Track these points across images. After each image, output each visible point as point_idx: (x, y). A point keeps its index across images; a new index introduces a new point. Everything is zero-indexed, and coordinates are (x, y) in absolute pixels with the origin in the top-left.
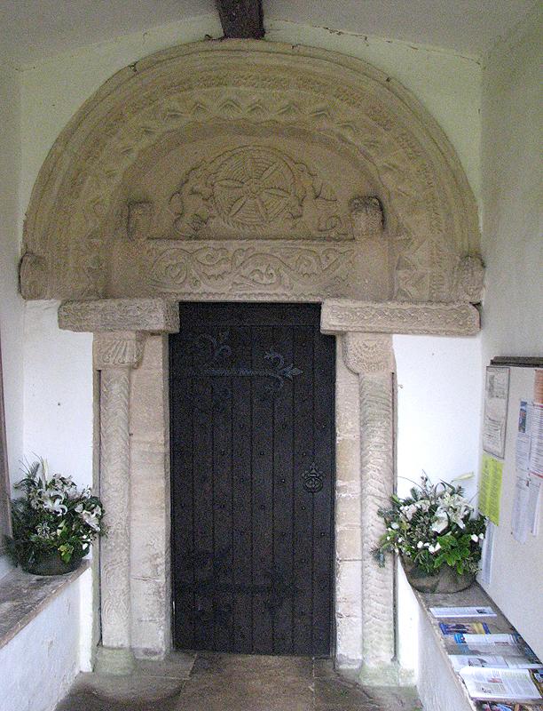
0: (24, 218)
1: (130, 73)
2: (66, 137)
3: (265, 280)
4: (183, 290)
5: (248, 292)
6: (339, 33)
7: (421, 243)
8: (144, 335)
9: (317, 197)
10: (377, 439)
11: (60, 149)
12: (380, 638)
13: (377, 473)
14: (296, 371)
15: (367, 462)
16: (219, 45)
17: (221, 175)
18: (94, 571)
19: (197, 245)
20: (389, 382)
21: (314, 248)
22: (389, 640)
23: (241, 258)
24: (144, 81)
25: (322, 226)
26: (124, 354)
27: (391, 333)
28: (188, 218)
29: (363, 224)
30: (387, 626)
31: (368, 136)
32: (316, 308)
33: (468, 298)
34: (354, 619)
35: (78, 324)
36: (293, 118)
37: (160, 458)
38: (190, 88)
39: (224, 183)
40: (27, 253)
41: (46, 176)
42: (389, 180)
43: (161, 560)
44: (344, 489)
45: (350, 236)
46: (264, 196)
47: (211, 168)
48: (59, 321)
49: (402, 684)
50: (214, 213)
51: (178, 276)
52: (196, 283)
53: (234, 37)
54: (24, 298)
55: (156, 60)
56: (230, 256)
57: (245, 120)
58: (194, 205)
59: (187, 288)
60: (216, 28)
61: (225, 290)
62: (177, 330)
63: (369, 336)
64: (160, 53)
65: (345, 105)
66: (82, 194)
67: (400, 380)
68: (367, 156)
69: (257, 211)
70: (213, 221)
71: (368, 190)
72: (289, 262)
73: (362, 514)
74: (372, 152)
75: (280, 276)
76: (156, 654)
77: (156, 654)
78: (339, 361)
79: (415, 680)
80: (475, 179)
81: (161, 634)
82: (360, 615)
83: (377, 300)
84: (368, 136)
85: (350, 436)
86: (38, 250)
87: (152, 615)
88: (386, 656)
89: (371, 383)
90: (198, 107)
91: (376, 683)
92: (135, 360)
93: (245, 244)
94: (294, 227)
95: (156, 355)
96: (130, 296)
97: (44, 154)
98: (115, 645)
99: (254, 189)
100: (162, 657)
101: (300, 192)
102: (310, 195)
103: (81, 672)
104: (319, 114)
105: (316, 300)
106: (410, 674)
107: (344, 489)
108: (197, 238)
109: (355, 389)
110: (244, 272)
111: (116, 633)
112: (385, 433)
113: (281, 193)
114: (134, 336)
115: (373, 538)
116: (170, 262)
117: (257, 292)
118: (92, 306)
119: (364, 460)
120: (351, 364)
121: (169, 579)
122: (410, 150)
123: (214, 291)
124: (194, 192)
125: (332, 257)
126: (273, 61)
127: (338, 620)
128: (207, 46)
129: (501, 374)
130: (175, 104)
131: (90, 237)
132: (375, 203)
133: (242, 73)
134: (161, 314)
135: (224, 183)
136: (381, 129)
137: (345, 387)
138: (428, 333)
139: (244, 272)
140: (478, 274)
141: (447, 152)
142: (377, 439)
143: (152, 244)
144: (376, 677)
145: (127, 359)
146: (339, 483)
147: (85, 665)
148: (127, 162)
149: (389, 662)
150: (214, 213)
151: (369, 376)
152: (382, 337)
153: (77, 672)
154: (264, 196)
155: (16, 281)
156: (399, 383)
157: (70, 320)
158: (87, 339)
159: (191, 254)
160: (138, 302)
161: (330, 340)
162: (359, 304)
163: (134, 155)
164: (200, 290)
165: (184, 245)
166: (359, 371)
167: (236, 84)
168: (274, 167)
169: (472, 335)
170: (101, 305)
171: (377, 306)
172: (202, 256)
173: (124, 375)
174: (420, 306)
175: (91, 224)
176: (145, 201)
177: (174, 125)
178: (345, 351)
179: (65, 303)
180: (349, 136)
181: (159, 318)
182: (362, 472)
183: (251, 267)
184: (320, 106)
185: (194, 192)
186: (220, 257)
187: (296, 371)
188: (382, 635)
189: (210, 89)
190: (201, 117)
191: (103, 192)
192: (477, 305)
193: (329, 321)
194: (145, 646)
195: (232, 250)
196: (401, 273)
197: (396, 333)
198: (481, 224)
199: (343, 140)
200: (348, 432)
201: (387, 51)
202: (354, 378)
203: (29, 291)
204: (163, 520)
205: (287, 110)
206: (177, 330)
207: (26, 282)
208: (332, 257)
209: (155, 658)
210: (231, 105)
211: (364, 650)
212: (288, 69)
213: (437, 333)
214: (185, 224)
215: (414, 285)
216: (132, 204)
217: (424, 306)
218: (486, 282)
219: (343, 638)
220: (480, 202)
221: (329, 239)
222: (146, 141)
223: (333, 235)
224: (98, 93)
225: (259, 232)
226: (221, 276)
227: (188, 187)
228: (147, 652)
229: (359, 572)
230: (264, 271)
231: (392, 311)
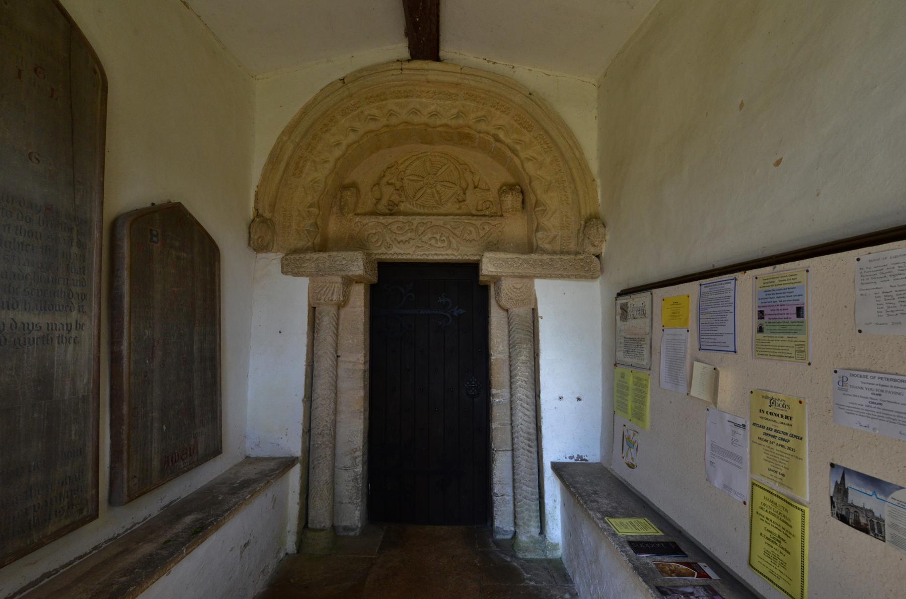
0: (256, 189)
1: (340, 84)
2: (290, 130)
3: (439, 244)
4: (380, 251)
5: (427, 253)
6: (494, 63)
7: (554, 213)
8: (349, 282)
9: (475, 187)
10: (523, 358)
11: (285, 138)
12: (530, 516)
13: (524, 383)
14: (462, 311)
15: (516, 375)
16: (406, 65)
17: (408, 172)
18: (302, 465)
19: (390, 219)
20: (531, 314)
21: (474, 222)
22: (536, 517)
23: (422, 229)
24: (352, 90)
25: (480, 208)
26: (333, 294)
27: (532, 277)
28: (384, 202)
29: (509, 203)
30: (535, 506)
31: (515, 136)
32: (475, 267)
33: (593, 250)
34: (507, 498)
35: (296, 270)
36: (461, 121)
37: (360, 374)
38: (386, 99)
39: (410, 177)
40: (258, 215)
41: (274, 159)
42: (530, 167)
43: (359, 453)
44: (497, 395)
45: (499, 214)
46: (439, 187)
47: (402, 167)
48: (282, 267)
49: (550, 556)
50: (404, 199)
51: (377, 241)
52: (389, 247)
53: (419, 59)
54: (255, 250)
55: (361, 74)
56: (414, 227)
57: (427, 125)
58: (388, 193)
59: (383, 250)
60: (405, 53)
61: (410, 251)
62: (375, 280)
63: (518, 280)
64: (361, 71)
65: (498, 113)
66: (304, 175)
67: (541, 312)
68: (514, 151)
69: (433, 196)
70: (402, 204)
71: (512, 180)
72: (456, 231)
73: (512, 415)
74: (518, 147)
75: (450, 242)
76: (353, 530)
77: (353, 530)
78: (493, 302)
79: (560, 553)
80: (594, 166)
81: (357, 513)
82: (512, 494)
83: (523, 253)
84: (515, 136)
85: (500, 356)
86: (267, 215)
87: (351, 498)
88: (535, 531)
89: (518, 316)
90: (391, 114)
91: (529, 556)
92: (342, 299)
93: (426, 219)
94: (460, 208)
95: (359, 298)
96: (339, 250)
97: (273, 142)
98: (318, 527)
99: (432, 182)
100: (358, 532)
101: (464, 185)
102: (471, 186)
103: (287, 554)
104: (479, 120)
105: (476, 258)
106: (555, 546)
107: (497, 395)
108: (391, 215)
109: (504, 321)
110: (424, 239)
111: (320, 515)
112: (529, 353)
113: (449, 184)
114: (340, 280)
115: (523, 434)
116: (371, 231)
117: (433, 252)
118: (308, 256)
119: (513, 373)
120: (503, 302)
121: (366, 467)
122: (545, 146)
123: (402, 252)
124: (388, 184)
125: (487, 228)
126: (448, 79)
127: (495, 498)
128: (395, 66)
129: (623, 300)
130: (375, 112)
131: (309, 207)
132: (518, 188)
133: (423, 89)
134: (361, 263)
135: (410, 177)
136: (525, 131)
137: (496, 317)
138: (561, 277)
139: (424, 239)
140: (601, 230)
141: (575, 145)
142: (523, 358)
143: (357, 219)
144: (527, 550)
145: (335, 298)
146: (494, 391)
147: (290, 545)
148: (338, 153)
149: (537, 536)
150: (404, 199)
151: (515, 311)
152: (526, 280)
153: (282, 555)
154: (439, 187)
155: (246, 235)
156: (540, 314)
157: (290, 268)
158: (303, 283)
159: (385, 226)
160: (344, 254)
161: (485, 288)
162: (509, 256)
163: (343, 147)
164: (392, 251)
165: (381, 219)
166: (508, 306)
167: (419, 96)
168: (445, 167)
169: (593, 277)
170: (315, 256)
171: (524, 257)
172: (394, 227)
173: (333, 310)
174: (555, 257)
175: (310, 198)
176: (354, 185)
177: (373, 126)
178: (498, 294)
179: (287, 255)
180: (502, 135)
181: (356, 264)
182: (511, 383)
183: (430, 235)
184: (480, 114)
185: (388, 184)
186: (407, 228)
187: (462, 311)
188: (532, 514)
189: (401, 100)
190: (394, 121)
191: (318, 174)
192: (598, 256)
193: (488, 268)
194: (344, 524)
195: (415, 223)
196: (540, 235)
197: (538, 277)
198: (599, 197)
199: (498, 140)
200: (500, 353)
201: (531, 75)
202: (503, 314)
203: (259, 246)
204: (361, 421)
205: (457, 116)
206: (375, 280)
207: (255, 237)
208: (487, 228)
209: (352, 534)
210: (416, 112)
211: (515, 524)
212: (457, 84)
213: (568, 277)
214: (382, 207)
215: (550, 243)
216: (346, 187)
217: (558, 256)
218: (607, 237)
219: (499, 513)
220: (598, 181)
221: (484, 216)
222: (352, 137)
223: (487, 213)
224: (315, 99)
225: (435, 211)
226: (408, 241)
227: (385, 180)
228: (346, 529)
229: (510, 460)
230: (438, 238)
231: (535, 261)
